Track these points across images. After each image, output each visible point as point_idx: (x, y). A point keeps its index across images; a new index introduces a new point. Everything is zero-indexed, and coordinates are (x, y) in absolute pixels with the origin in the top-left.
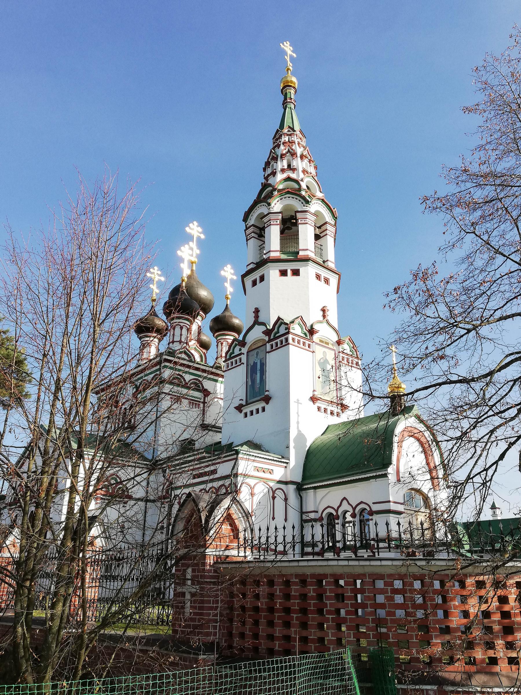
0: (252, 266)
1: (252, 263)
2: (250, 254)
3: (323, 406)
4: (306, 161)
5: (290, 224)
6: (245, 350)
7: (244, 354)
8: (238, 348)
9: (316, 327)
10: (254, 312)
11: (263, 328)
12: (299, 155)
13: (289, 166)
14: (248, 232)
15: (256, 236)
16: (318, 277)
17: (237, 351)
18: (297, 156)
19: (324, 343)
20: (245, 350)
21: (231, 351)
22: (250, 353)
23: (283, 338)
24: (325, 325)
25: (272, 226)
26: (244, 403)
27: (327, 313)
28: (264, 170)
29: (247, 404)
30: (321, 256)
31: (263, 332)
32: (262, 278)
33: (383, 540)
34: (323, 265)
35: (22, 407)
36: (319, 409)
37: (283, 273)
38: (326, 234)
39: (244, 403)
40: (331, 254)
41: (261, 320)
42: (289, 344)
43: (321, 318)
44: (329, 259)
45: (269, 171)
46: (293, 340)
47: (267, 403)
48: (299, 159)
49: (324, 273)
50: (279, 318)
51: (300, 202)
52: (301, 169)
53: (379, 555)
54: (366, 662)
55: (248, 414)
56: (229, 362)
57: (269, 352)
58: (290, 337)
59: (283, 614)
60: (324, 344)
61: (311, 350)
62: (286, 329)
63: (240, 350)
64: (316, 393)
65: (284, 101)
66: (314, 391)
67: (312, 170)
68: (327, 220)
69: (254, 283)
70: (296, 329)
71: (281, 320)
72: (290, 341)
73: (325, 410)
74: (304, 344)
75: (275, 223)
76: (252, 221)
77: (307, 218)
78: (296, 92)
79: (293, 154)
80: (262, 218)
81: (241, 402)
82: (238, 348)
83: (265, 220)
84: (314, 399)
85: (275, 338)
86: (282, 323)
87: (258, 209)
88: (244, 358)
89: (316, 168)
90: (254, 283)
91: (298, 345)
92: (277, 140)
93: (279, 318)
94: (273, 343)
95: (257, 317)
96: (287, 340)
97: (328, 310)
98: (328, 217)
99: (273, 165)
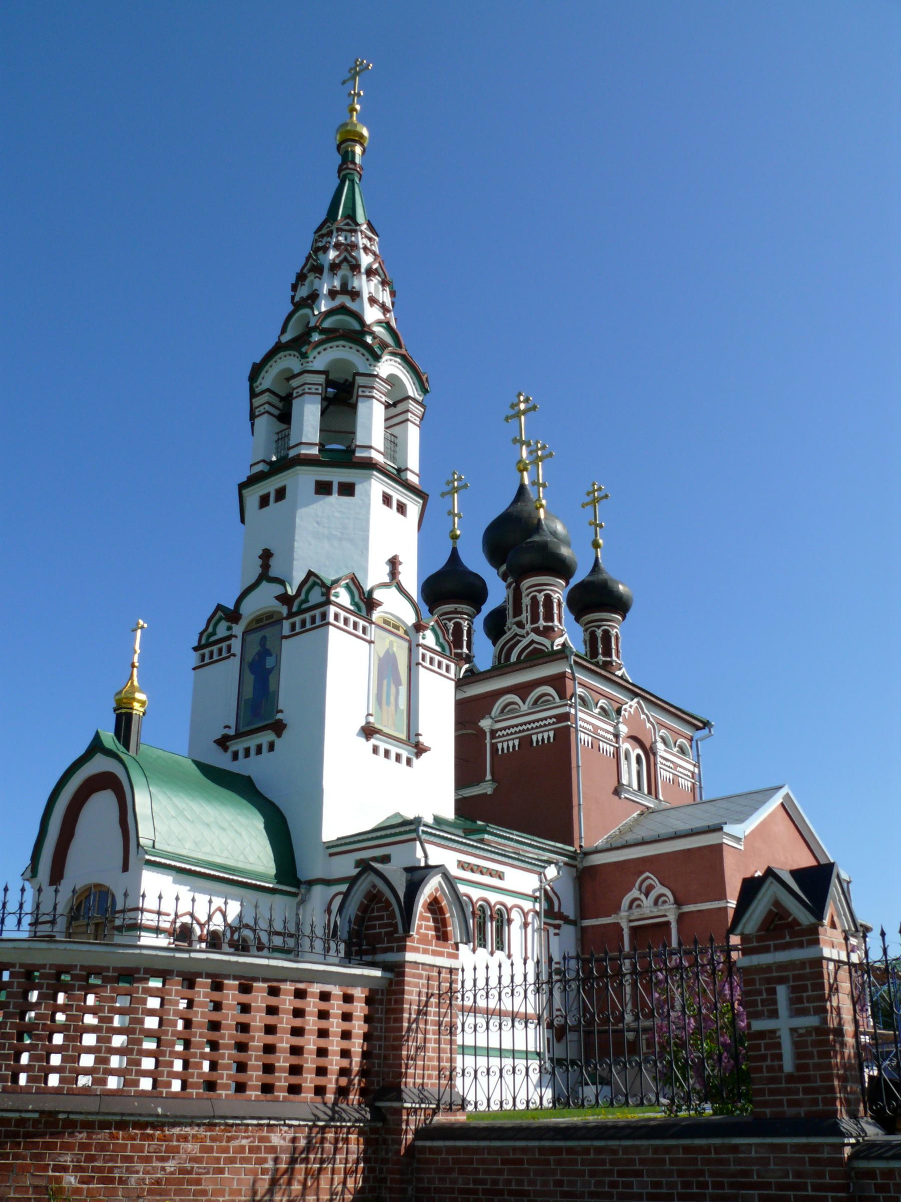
0: (261, 467)
1: (264, 461)
2: (254, 445)
3: (383, 746)
4: (376, 280)
5: (342, 397)
6: (238, 629)
7: (236, 637)
8: (223, 625)
9: (377, 595)
10: (260, 557)
11: (277, 589)
12: (363, 270)
13: (344, 285)
14: (257, 401)
15: (276, 412)
16: (387, 500)
17: (222, 631)
18: (360, 271)
19: (391, 626)
20: (238, 629)
21: (210, 630)
22: (249, 638)
23: (317, 612)
24: (393, 590)
25: (306, 396)
26: (232, 732)
27: (401, 568)
28: (294, 287)
29: (239, 735)
30: (393, 459)
31: (278, 598)
32: (281, 494)
33: (278, 934)
34: (398, 476)
35: (311, 883)
36: (375, 750)
37: (323, 488)
38: (408, 420)
39: (232, 732)
40: (413, 461)
41: (273, 573)
42: (329, 623)
43: (387, 579)
44: (409, 466)
45: (303, 292)
46: (336, 617)
47: (279, 735)
48: (364, 277)
49: (398, 494)
50: (310, 574)
51: (364, 358)
52: (365, 296)
53: (168, 915)
54: (55, 999)
55: (241, 754)
56: (206, 651)
57: (286, 637)
58: (333, 609)
59: (23, 980)
60: (391, 628)
61: (368, 638)
62: (323, 595)
63: (229, 628)
64: (371, 719)
65: (340, 166)
66: (369, 715)
67: (385, 297)
68: (411, 394)
69: (264, 501)
70: (343, 597)
71: (312, 579)
72: (331, 619)
73: (387, 754)
74: (355, 626)
75: (313, 391)
76: (267, 380)
77: (373, 388)
78: (364, 152)
79: (355, 267)
80: (288, 379)
81: (226, 731)
82: (223, 625)
83: (294, 383)
84: (368, 732)
85: (301, 612)
86: (315, 584)
87: (279, 361)
88: (236, 645)
89: (393, 294)
90: (264, 501)
91: (345, 627)
92: (322, 236)
93: (310, 574)
94: (297, 619)
95: (266, 566)
96: (324, 616)
97: (401, 563)
98: (411, 389)
99: (312, 283)
